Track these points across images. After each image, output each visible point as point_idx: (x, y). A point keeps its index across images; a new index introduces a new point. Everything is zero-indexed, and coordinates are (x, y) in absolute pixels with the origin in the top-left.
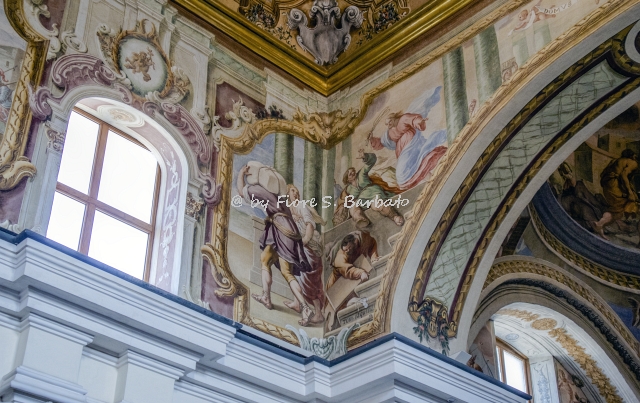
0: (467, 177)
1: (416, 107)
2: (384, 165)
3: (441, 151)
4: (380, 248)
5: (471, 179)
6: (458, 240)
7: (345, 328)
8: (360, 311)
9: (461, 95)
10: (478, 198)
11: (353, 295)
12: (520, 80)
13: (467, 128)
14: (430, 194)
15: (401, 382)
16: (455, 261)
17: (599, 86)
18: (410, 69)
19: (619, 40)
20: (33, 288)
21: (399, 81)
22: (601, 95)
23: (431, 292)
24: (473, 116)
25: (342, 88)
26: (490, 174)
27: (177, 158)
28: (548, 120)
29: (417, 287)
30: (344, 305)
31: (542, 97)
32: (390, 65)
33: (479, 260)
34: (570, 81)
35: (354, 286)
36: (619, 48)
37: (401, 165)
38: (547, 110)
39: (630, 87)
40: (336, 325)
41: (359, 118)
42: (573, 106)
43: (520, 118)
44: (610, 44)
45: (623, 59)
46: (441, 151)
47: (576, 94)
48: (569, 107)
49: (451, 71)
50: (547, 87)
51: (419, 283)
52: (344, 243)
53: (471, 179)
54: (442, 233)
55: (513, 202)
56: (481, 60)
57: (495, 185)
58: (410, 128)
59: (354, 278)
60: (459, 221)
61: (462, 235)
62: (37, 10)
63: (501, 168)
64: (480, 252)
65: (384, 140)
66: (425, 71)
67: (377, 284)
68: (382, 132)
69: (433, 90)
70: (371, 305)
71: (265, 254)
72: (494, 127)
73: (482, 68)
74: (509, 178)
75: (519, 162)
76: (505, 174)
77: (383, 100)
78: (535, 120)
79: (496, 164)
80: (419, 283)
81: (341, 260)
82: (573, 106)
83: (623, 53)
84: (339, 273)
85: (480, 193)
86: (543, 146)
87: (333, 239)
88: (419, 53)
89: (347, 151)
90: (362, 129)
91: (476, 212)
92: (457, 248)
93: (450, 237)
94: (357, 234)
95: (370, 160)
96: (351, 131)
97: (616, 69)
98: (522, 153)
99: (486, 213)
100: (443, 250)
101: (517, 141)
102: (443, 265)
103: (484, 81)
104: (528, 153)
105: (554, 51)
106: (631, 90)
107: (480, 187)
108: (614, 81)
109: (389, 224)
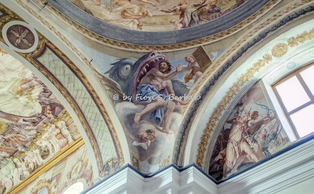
0: (80, 119)
5: (81, 118)
6: (100, 134)
10: (89, 118)
16: (106, 140)
17: (51, 59)
19: (26, 55)
22: (56, 57)
26: (83, 109)
28: (67, 79)
29: (99, 164)
31: (54, 82)
33: (113, 128)
34: (47, 71)
36: (30, 55)
38: (61, 80)
39: (52, 47)
42: (61, 69)
43: (63, 92)
44: (28, 58)
45: (37, 52)
47: (55, 68)
48: (61, 71)
50: (50, 80)
51: (99, 163)
53: (81, 118)
54: (93, 140)
55: (100, 101)
57: (88, 108)
60: (93, 130)
61: (99, 131)
62: (187, 84)
63: (83, 103)
64: (111, 126)
74: (89, 100)
75: (83, 94)
76: (86, 102)
78: (65, 85)
79: (80, 105)
80: (99, 163)
82: (61, 69)
83: (32, 53)
86: (79, 81)
91: (95, 120)
92: (102, 136)
93: (96, 137)
98: (80, 92)
99: (98, 116)
100: (98, 143)
101: (73, 94)
102: (103, 146)
104: (81, 89)
106: (54, 45)
107: (86, 115)
108: (48, 54)
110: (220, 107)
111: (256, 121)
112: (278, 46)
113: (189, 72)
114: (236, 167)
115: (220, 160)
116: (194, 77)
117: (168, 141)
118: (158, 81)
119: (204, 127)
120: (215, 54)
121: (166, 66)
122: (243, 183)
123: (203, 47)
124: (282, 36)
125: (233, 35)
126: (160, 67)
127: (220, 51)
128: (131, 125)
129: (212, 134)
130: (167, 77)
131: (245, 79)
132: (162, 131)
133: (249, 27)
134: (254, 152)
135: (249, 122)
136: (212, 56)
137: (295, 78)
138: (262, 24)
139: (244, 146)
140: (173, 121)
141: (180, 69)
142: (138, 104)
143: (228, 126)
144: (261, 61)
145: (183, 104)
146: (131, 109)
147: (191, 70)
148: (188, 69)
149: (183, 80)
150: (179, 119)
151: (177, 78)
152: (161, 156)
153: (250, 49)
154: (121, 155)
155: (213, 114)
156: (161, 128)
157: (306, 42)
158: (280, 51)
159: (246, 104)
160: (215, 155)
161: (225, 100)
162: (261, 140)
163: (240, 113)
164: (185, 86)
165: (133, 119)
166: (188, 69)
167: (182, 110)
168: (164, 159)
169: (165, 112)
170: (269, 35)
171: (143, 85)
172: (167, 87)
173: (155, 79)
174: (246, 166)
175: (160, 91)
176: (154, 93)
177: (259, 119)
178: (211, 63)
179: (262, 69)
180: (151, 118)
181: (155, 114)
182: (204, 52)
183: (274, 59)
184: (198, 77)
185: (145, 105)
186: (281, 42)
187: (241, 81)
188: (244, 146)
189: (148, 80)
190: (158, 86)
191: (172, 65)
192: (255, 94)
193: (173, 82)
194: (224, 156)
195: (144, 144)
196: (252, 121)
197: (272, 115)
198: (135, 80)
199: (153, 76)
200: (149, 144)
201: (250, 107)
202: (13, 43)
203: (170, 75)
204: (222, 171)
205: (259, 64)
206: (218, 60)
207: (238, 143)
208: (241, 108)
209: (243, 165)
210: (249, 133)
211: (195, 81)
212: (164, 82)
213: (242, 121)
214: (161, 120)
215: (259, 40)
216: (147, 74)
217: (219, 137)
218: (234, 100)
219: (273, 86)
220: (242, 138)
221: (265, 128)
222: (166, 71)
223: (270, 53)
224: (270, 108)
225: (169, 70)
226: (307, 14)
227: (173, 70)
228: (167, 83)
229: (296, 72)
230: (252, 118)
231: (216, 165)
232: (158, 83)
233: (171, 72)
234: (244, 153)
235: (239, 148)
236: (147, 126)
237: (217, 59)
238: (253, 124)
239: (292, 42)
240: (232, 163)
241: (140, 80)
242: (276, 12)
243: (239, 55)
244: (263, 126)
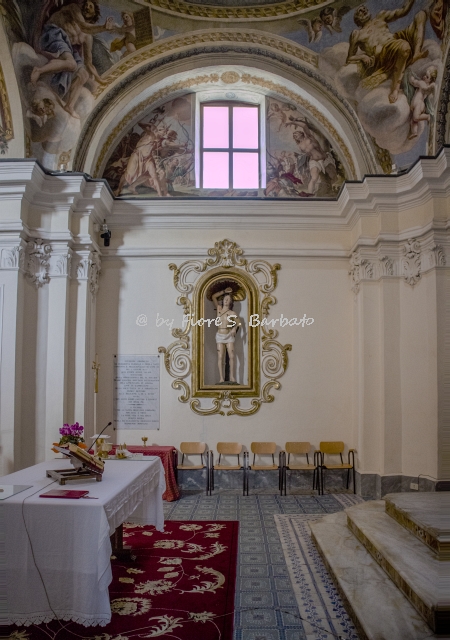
32: (369, 560)
110: (141, 106)
111: (172, 144)
112: (232, 73)
113: (122, 37)
114: (135, 186)
115: (118, 167)
116: (124, 49)
117: (72, 127)
118: (75, 29)
119: (115, 125)
120: (161, 32)
121: (93, 10)
122: (142, 210)
123: (151, 12)
124: (241, 67)
125: (194, 21)
126: (83, 7)
127: (169, 32)
128: (26, 83)
129: (119, 134)
130: (89, 29)
131: (180, 85)
132: (64, 108)
133: (216, 25)
134: (158, 179)
135: (164, 141)
136: (157, 34)
137: (225, 110)
138: (230, 34)
139: (149, 167)
140: (81, 99)
141: (110, 26)
142: (40, 53)
143: (139, 130)
144: (207, 77)
145: (99, 82)
146: (29, 58)
147: (123, 36)
148: (119, 31)
149: (108, 45)
150: (90, 102)
151: (101, 36)
152: (59, 143)
153: (202, 55)
154: (8, 125)
155: (130, 112)
156: (64, 104)
157: (257, 86)
158: (230, 79)
159: (168, 116)
160: (113, 159)
161: (148, 101)
162: (169, 169)
163: (157, 122)
164: (108, 56)
165: (29, 75)
166: (119, 31)
167: (97, 91)
168: (64, 150)
169: (74, 80)
170: (229, 53)
171: (54, 25)
172: (85, 44)
173: (71, 23)
174: (145, 189)
175: (73, 46)
176: (65, 45)
177: (174, 144)
178: (151, 42)
179: (203, 84)
180: (52, 82)
181: (59, 79)
182: (149, 20)
183: (220, 82)
184: (129, 51)
185: (50, 58)
186: (236, 71)
187: (175, 86)
188: (149, 167)
189: (62, 20)
190: (73, 36)
191: (102, 14)
192: (182, 109)
193: (95, 41)
194: (125, 166)
195: (38, 117)
196: (168, 142)
197: (190, 147)
198: (43, 11)
199: (71, 17)
200: (45, 121)
201: (170, 122)
203: (94, 28)
204: (119, 181)
205: (202, 79)
206: (163, 42)
207: (145, 160)
208: (160, 117)
209: (142, 186)
210: (160, 155)
211: (124, 56)
212: (84, 34)
213: (156, 134)
214: (66, 91)
215: (217, 51)
216: (64, 9)
217: (125, 139)
218: (156, 104)
219: (203, 104)
220: (151, 156)
221: (178, 157)
222: (89, 19)
223: (220, 75)
224: (191, 137)
225: (94, 19)
226: (275, 61)
227: (101, 23)
228: (86, 38)
229: (231, 103)
230: (169, 138)
231: (112, 172)
232: (74, 32)
233: (97, 24)
234: (146, 174)
235: (144, 166)
236: (46, 92)
237: (161, 42)
238: (167, 147)
239: (246, 78)
240: (132, 179)
241: (51, 14)
242: (251, 31)
243: (188, 54)
244: (177, 154)
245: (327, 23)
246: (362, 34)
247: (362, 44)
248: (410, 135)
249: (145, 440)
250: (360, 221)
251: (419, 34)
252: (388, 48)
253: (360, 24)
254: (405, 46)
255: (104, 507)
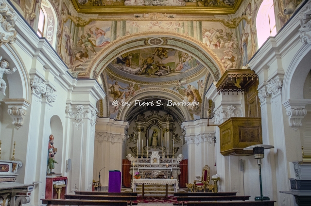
1: (104, 29)
2: (93, 39)
3: (109, 43)
4: (89, 57)
7: (78, 72)
8: (82, 69)
9: (115, 32)
11: (80, 65)
12: (130, 37)
13: (115, 41)
14: (104, 51)
15: (93, 88)
18: (103, 19)
20: (41, 51)
21: (100, 20)
23: (96, 70)
24: (118, 39)
25: (83, 13)
27: (53, 19)
30: (78, 66)
32: (98, 15)
35: (81, 63)
37: (98, 41)
38: (130, 44)
40: (75, 70)
41: (88, 23)
46: (109, 43)
49: (114, 25)
52: (79, 52)
56: (122, 27)
58: (101, 33)
59: (81, 61)
65: (94, 32)
66: (107, 21)
67: (88, 65)
68: (93, 30)
69: (108, 27)
70: (85, 69)
71: (66, 50)
72: (121, 43)
73: (121, 29)
77: (95, 22)
81: (78, 55)
84: (77, 59)
85: (111, 54)
87: (76, 50)
88: (106, 16)
89: (83, 30)
90: (88, 26)
94: (83, 52)
95: (90, 36)
96: (84, 26)
97: (145, 42)
101: (122, 47)
103: (121, 32)
105: (138, 35)
109: (92, 53)
202: (157, 39)
245: (112, 79)
246: (115, 86)
247: (113, 87)
248: (114, 111)
249: (41, 182)
250: (263, 73)
251: (123, 94)
252: (117, 92)
253: (116, 84)
254: (120, 94)
255: (292, 188)
